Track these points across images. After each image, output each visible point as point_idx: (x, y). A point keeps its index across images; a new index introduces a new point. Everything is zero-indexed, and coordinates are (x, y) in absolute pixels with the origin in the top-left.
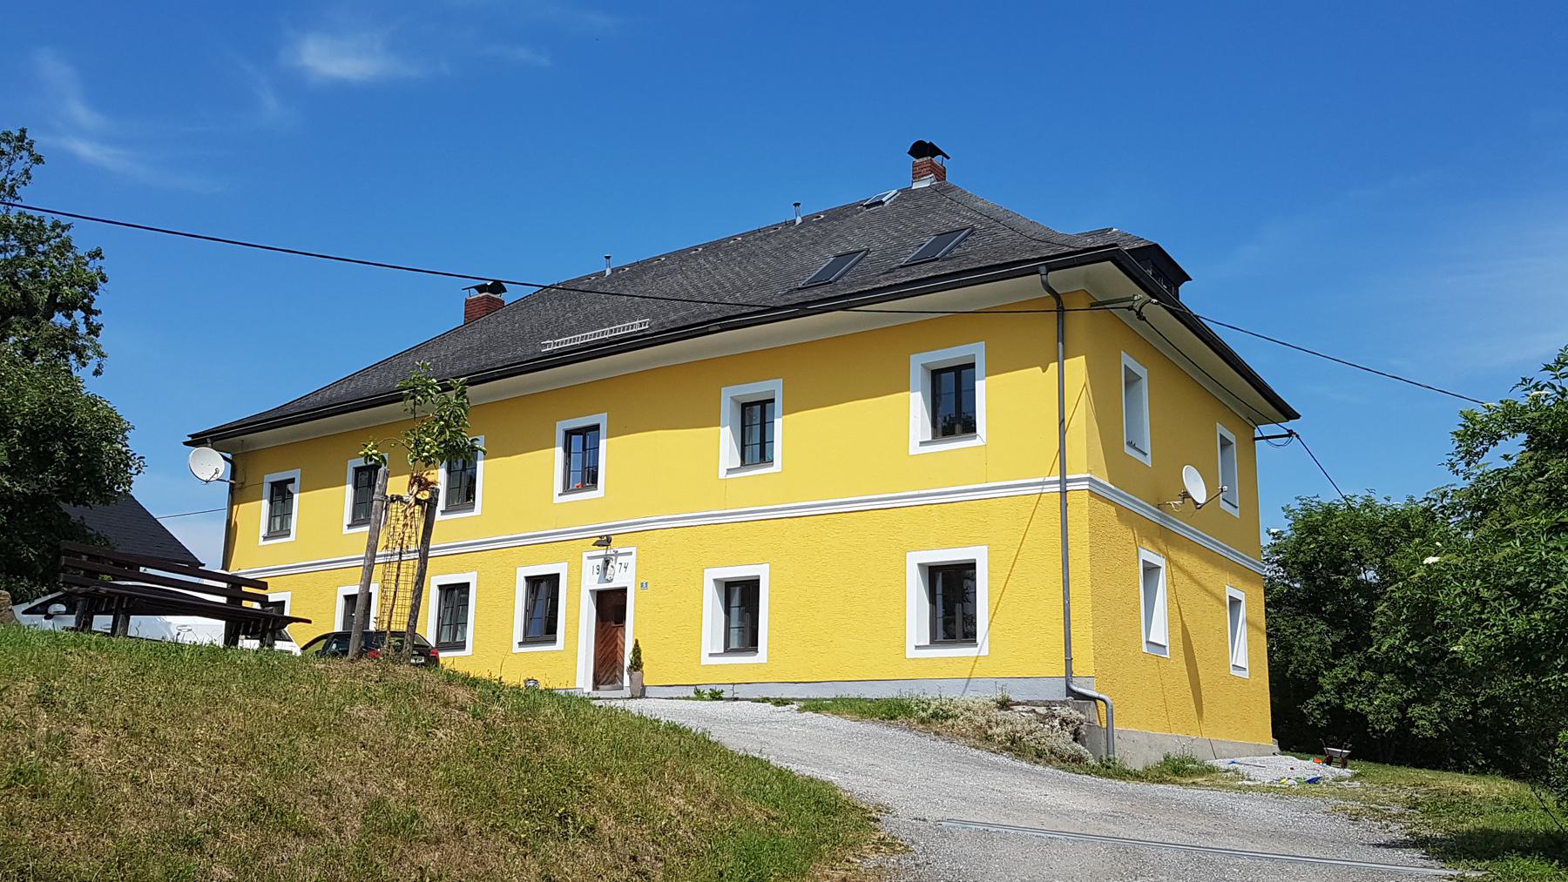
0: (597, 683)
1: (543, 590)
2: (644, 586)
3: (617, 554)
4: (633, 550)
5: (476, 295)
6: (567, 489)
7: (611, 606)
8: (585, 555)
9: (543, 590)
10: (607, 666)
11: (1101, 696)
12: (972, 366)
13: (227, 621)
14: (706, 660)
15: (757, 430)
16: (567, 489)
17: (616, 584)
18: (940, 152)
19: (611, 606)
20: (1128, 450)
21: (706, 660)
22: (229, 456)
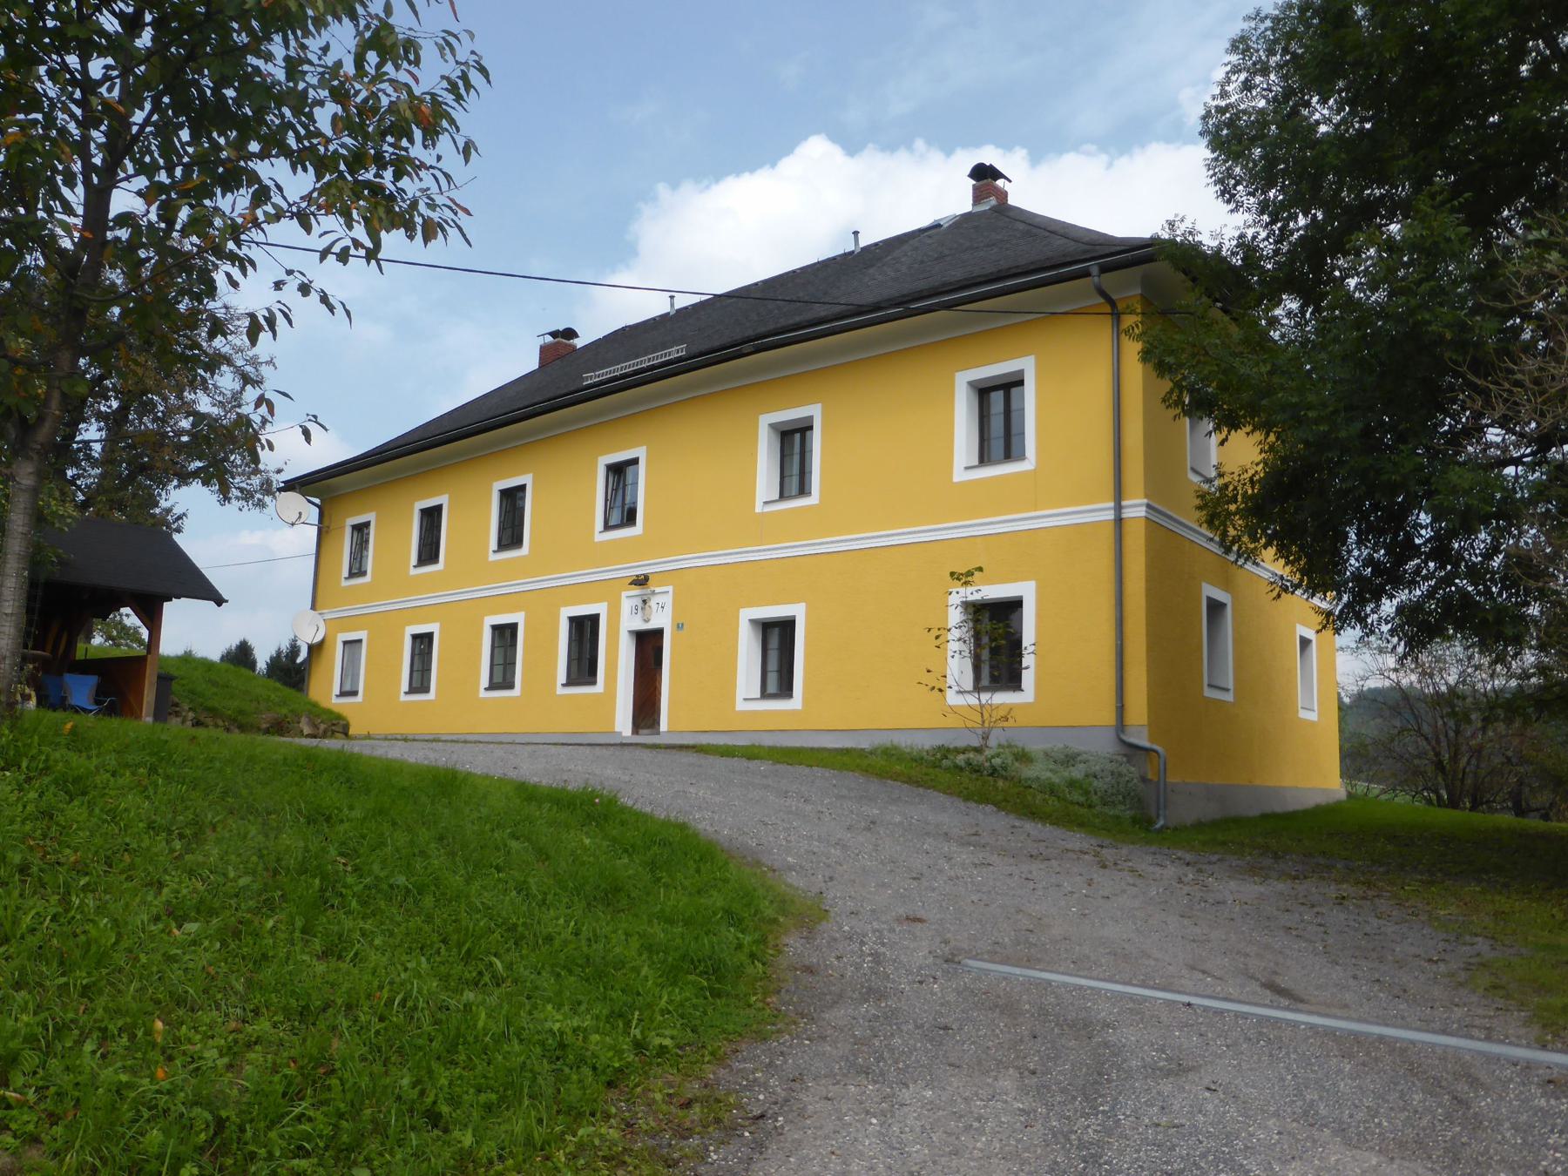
0: (637, 727)
1: (585, 631)
2: (680, 627)
3: (653, 593)
4: (670, 589)
5: (549, 339)
6: (607, 527)
7: (648, 644)
8: (624, 594)
9: (585, 631)
10: (646, 708)
11: (1155, 747)
12: (1021, 383)
13: (1036, 580)
14: (741, 706)
15: (796, 458)
16: (607, 527)
17: (653, 624)
18: (1002, 176)
19: (648, 644)
20: (1208, 693)
21: (741, 706)
22: (317, 501)
